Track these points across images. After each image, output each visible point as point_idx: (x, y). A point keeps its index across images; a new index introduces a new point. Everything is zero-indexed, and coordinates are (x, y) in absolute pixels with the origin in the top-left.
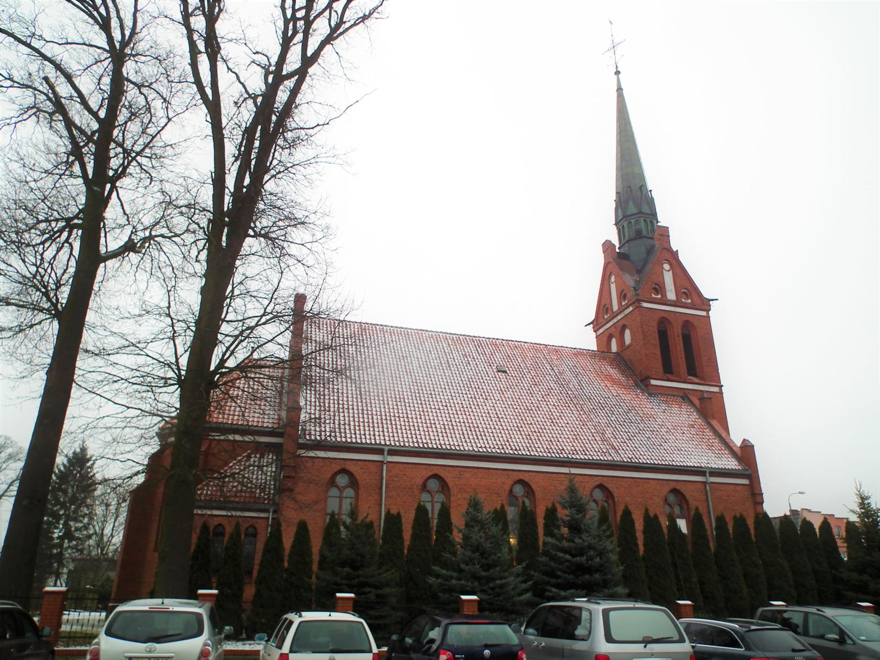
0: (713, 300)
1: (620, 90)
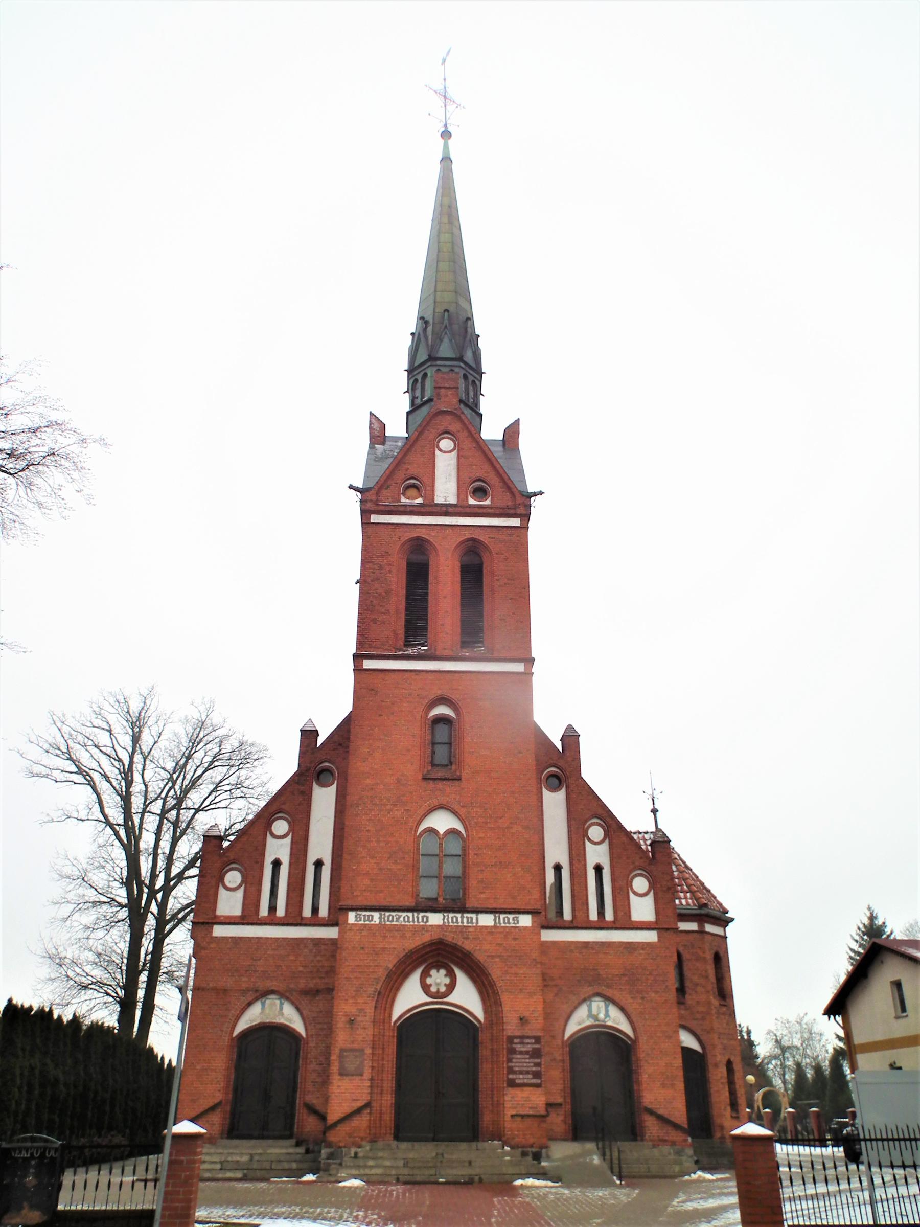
1: (446, 160)
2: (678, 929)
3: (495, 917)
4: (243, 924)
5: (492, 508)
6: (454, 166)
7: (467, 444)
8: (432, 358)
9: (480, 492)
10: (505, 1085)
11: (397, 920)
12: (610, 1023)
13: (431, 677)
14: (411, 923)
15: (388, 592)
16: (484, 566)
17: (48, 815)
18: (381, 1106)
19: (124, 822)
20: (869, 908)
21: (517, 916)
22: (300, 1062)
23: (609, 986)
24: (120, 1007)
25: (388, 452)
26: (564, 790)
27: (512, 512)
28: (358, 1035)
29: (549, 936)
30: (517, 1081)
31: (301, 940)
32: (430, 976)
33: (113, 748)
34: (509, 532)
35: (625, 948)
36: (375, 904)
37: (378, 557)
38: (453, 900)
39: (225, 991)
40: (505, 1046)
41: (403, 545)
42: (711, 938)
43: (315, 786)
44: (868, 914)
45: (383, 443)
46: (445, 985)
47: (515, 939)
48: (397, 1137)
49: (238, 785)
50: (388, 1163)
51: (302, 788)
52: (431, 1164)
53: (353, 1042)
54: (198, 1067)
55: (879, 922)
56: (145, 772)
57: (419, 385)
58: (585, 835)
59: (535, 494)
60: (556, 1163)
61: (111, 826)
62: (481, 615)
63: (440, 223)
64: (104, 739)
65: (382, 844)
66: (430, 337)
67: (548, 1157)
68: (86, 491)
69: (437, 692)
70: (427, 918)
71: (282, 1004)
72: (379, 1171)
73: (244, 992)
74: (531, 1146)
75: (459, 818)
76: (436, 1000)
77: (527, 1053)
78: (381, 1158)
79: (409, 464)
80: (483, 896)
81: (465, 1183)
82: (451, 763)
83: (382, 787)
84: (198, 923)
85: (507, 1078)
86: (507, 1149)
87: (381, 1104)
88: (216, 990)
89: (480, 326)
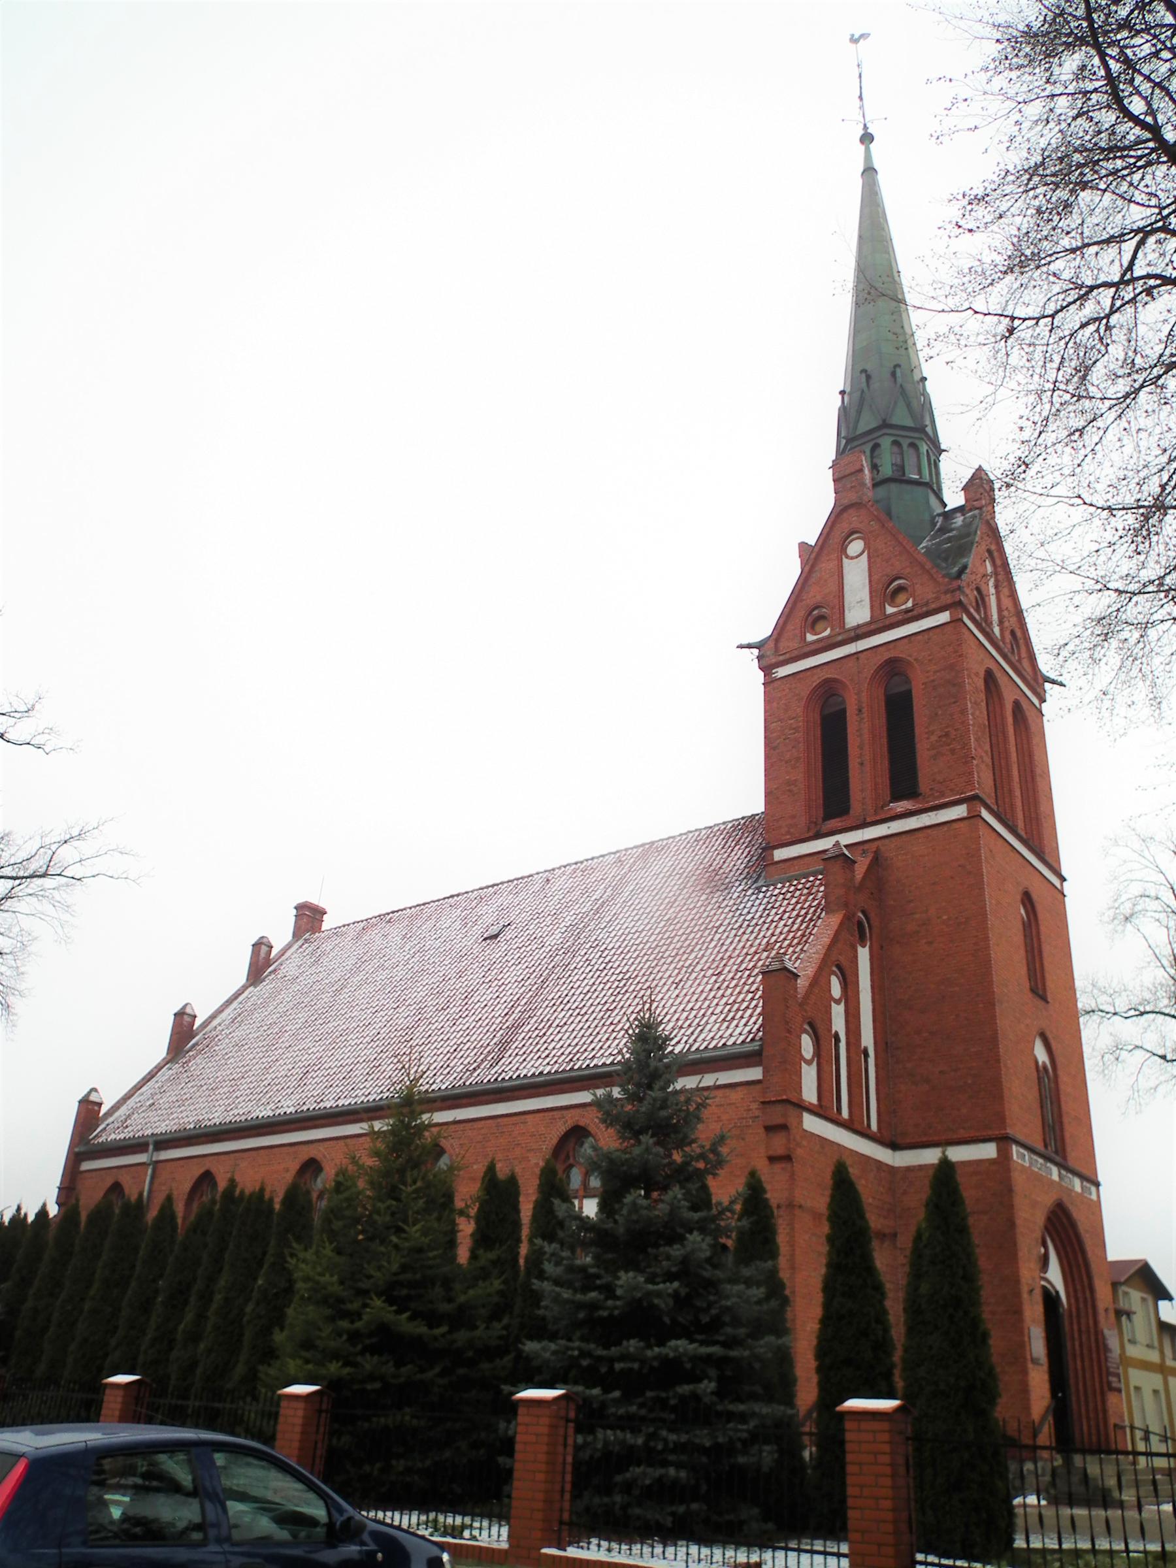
0: (1053, 682)
1: (869, 171)
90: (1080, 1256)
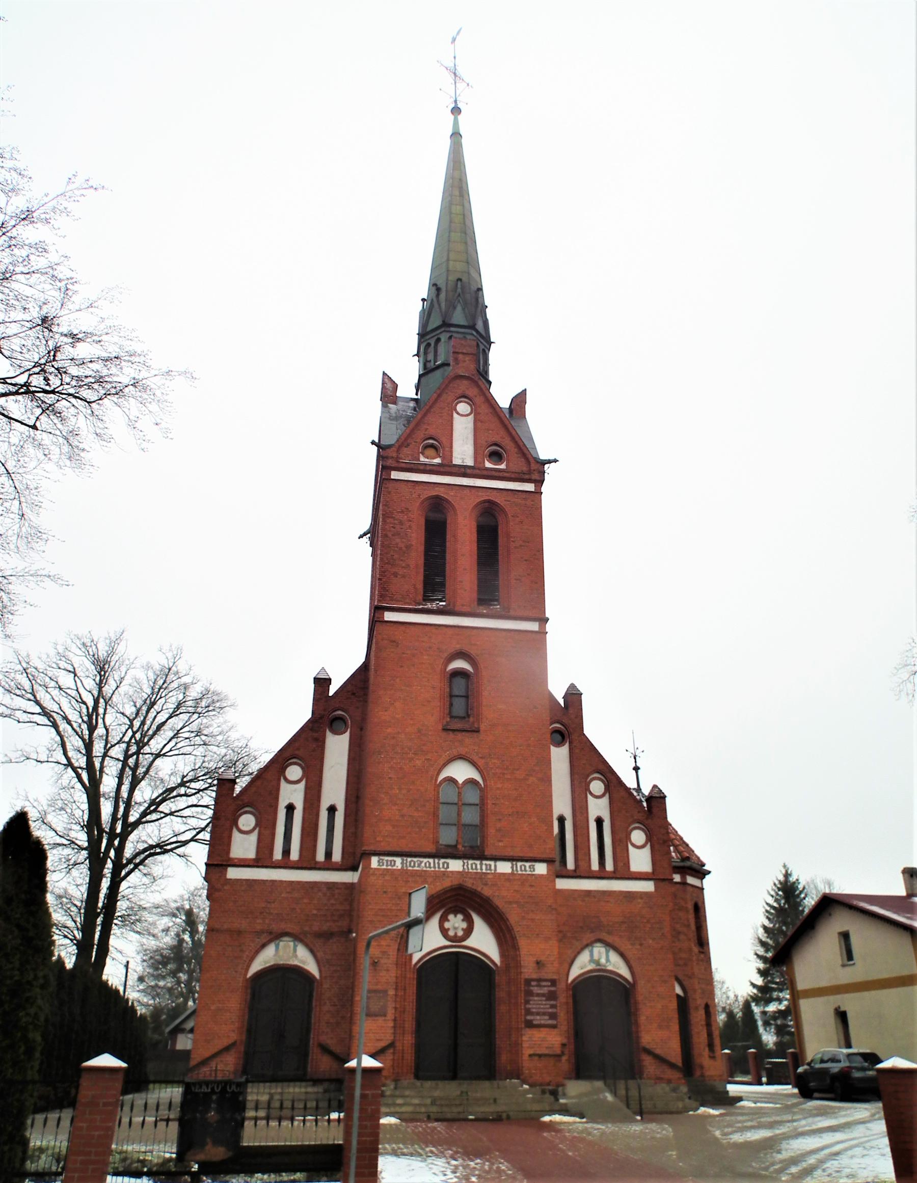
1: (456, 135)
2: (673, 879)
3: (513, 865)
4: (258, 867)
5: (508, 472)
6: (464, 141)
7: (484, 409)
8: (446, 325)
9: (496, 456)
10: (523, 1026)
11: (419, 866)
12: (610, 968)
13: (450, 632)
14: (432, 869)
15: (408, 547)
16: (499, 527)
17: (6, 755)
18: (403, 1046)
19: (87, 765)
20: (785, 866)
21: (533, 864)
22: (314, 1004)
23: (609, 933)
24: (77, 949)
25: (401, 412)
26: (567, 745)
27: (527, 477)
28: (382, 976)
29: (563, 884)
30: (535, 1022)
31: (315, 884)
32: (448, 921)
33: (77, 690)
34: (524, 496)
35: (625, 897)
36: (398, 849)
37: (398, 512)
38: (471, 847)
39: (239, 932)
40: (523, 989)
41: (422, 502)
42: (691, 889)
43: (329, 734)
44: (784, 872)
45: (395, 403)
46: (463, 929)
47: (531, 886)
48: (417, 1077)
49: (198, 733)
50: (416, 1101)
51: (315, 735)
52: (458, 1102)
53: (377, 984)
54: (213, 1008)
55: (792, 879)
56: (106, 715)
57: (432, 349)
58: (587, 789)
59: (549, 462)
60: (574, 1101)
61: (74, 769)
62: (496, 573)
63: (451, 195)
64: (67, 680)
65: (404, 792)
66: (443, 305)
67: (564, 1095)
68: (163, 425)
69: (456, 646)
70: (448, 864)
71: (295, 946)
72: (409, 1109)
73: (259, 933)
74: (549, 1084)
75: (477, 769)
76: (454, 944)
77: (543, 995)
78: (407, 1096)
79: (428, 424)
80: (501, 844)
81: (493, 1120)
82: (468, 716)
83: (403, 736)
84: (213, 865)
85: (525, 1019)
86: (526, 1086)
87: (403, 1043)
88: (230, 931)
89: (490, 297)
90: (766, 1100)
